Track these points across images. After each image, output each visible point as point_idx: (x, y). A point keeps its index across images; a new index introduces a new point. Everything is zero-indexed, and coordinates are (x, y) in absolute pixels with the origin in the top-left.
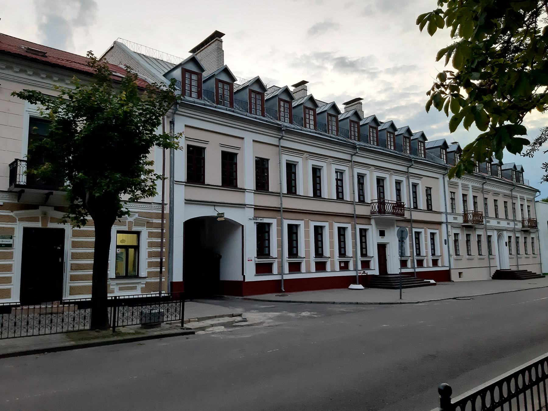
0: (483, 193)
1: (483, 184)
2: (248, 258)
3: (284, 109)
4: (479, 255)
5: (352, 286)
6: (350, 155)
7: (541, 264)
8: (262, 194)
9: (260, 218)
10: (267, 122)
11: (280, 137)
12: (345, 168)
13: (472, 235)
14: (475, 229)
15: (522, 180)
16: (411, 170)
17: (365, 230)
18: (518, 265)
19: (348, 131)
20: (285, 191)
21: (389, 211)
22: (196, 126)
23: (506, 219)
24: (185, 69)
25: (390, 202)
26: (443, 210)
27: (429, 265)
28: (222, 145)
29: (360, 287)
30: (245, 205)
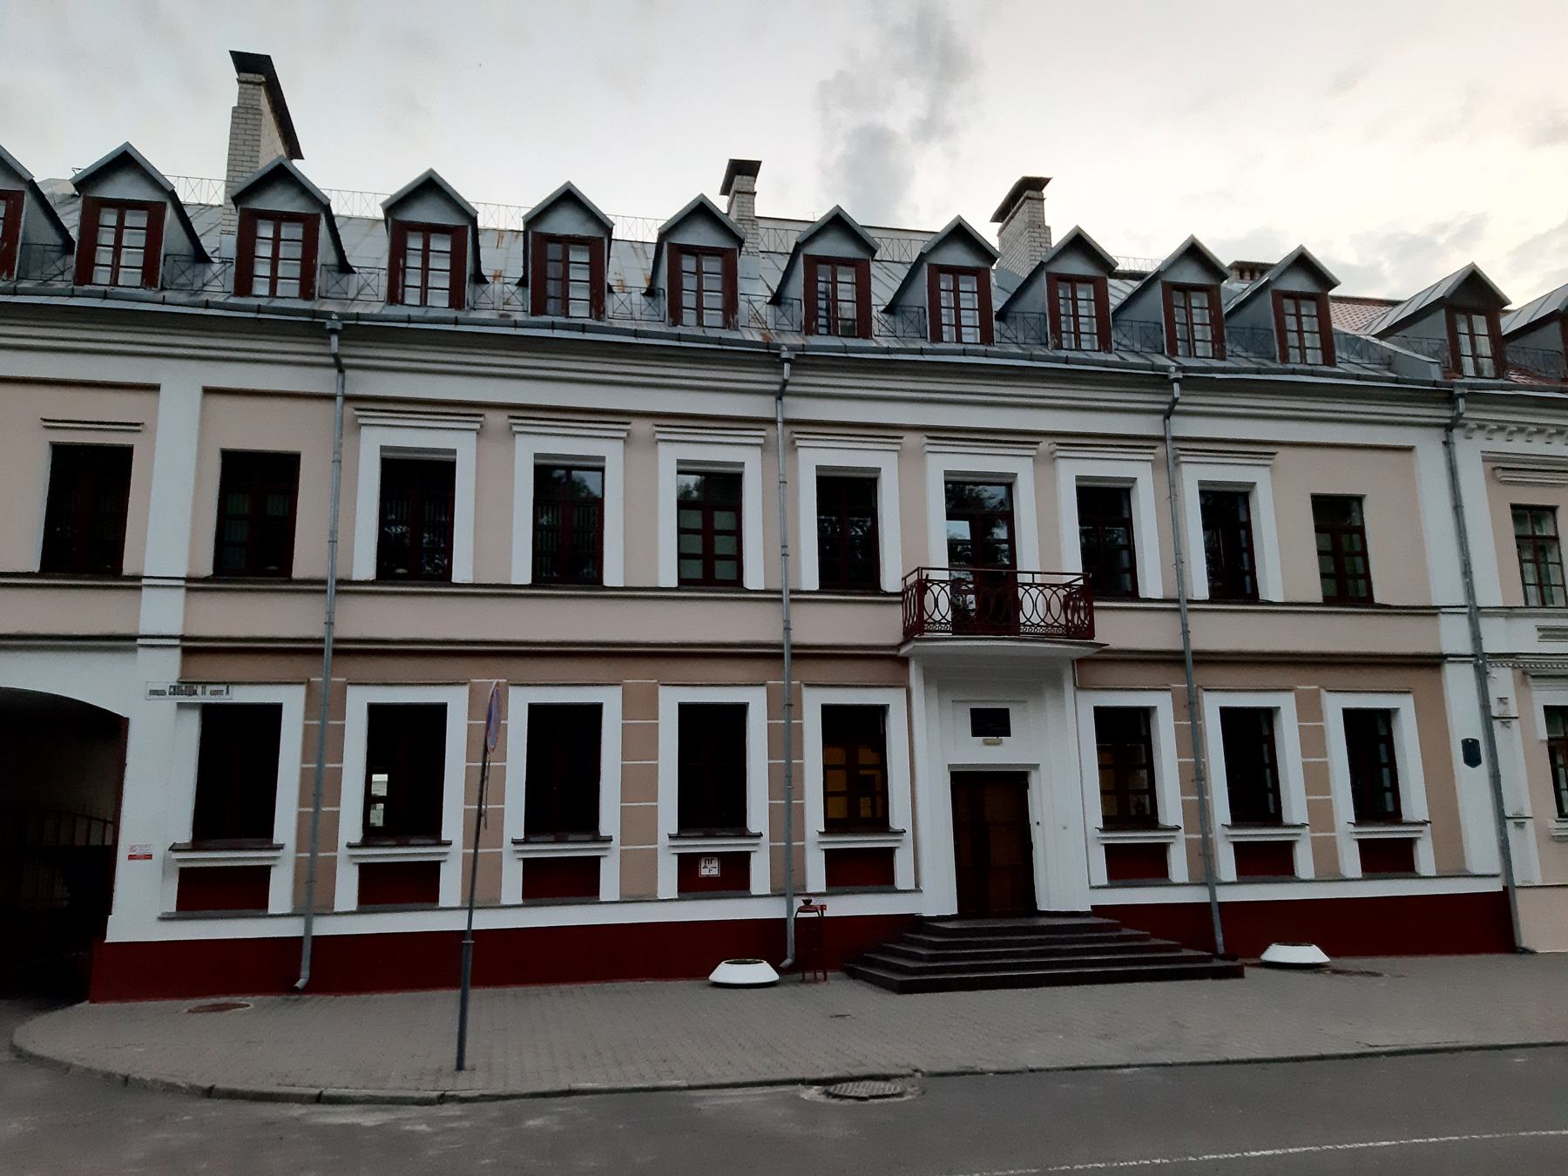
2: (132, 848)
3: (1299, 323)
5: (726, 972)
6: (773, 399)
9: (209, 688)
11: (1166, 407)
12: (1140, 472)
20: (1199, 586)
22: (1322, 441)
24: (1170, 283)
25: (1038, 579)
26: (1447, 590)
27: (1468, 868)
28: (50, 424)
29: (1312, 954)
30: (133, 638)
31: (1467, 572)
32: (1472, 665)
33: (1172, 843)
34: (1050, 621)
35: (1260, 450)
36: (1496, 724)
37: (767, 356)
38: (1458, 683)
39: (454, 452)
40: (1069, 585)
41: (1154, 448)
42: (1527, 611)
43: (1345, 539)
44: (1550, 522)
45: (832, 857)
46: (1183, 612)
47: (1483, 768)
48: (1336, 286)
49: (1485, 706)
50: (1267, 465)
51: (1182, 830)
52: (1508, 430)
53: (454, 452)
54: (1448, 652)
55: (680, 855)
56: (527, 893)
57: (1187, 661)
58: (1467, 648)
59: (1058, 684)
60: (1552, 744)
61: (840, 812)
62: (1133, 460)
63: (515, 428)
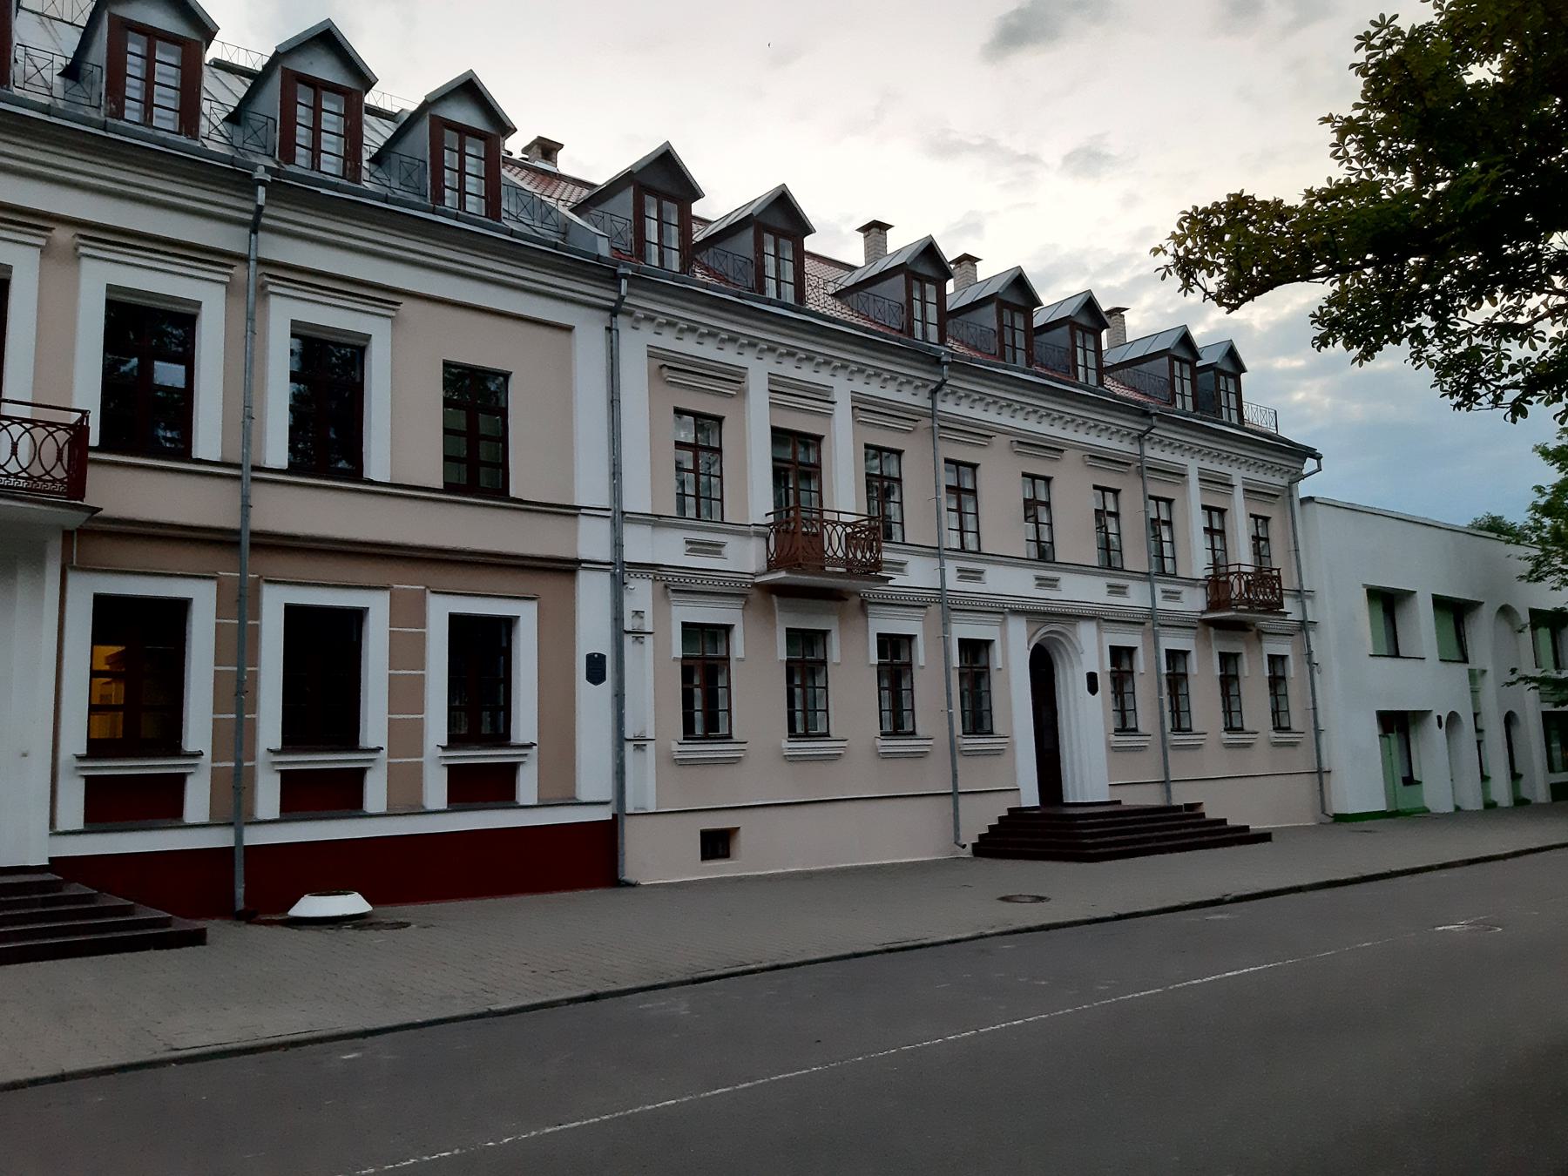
0: (1142, 477)
1: (934, 392)
4: (1230, 729)
5: (310, 906)
6: (247, 231)
7: (1321, 773)
8: (515, 509)
10: (511, 236)
13: (1244, 655)
14: (1260, 634)
15: (1233, 405)
16: (947, 406)
17: (1236, 656)
18: (1166, 783)
19: (102, 71)
21: (840, 554)
23: (1110, 567)
26: (590, 489)
29: (354, 904)
31: (616, 473)
32: (609, 574)
33: (522, 762)
34: (37, 471)
35: (385, 298)
36: (628, 639)
37: (237, 179)
38: (592, 591)
39: (198, 304)
40: (854, 524)
41: (231, 267)
42: (682, 521)
43: (483, 418)
44: (895, 463)
45: (93, 785)
46: (244, 481)
47: (607, 687)
48: (812, 233)
49: (618, 618)
50: (389, 317)
51: (384, 752)
52: (797, 357)
53: (198, 304)
54: (584, 558)
55: (283, 773)
56: (452, 797)
57: (243, 543)
58: (605, 554)
59: (36, 561)
60: (791, 665)
61: (111, 727)
62: (95, 257)
63: (82, 250)
